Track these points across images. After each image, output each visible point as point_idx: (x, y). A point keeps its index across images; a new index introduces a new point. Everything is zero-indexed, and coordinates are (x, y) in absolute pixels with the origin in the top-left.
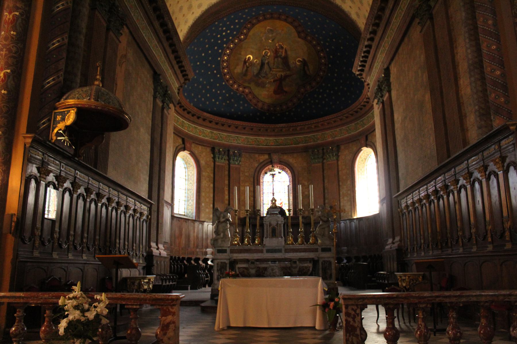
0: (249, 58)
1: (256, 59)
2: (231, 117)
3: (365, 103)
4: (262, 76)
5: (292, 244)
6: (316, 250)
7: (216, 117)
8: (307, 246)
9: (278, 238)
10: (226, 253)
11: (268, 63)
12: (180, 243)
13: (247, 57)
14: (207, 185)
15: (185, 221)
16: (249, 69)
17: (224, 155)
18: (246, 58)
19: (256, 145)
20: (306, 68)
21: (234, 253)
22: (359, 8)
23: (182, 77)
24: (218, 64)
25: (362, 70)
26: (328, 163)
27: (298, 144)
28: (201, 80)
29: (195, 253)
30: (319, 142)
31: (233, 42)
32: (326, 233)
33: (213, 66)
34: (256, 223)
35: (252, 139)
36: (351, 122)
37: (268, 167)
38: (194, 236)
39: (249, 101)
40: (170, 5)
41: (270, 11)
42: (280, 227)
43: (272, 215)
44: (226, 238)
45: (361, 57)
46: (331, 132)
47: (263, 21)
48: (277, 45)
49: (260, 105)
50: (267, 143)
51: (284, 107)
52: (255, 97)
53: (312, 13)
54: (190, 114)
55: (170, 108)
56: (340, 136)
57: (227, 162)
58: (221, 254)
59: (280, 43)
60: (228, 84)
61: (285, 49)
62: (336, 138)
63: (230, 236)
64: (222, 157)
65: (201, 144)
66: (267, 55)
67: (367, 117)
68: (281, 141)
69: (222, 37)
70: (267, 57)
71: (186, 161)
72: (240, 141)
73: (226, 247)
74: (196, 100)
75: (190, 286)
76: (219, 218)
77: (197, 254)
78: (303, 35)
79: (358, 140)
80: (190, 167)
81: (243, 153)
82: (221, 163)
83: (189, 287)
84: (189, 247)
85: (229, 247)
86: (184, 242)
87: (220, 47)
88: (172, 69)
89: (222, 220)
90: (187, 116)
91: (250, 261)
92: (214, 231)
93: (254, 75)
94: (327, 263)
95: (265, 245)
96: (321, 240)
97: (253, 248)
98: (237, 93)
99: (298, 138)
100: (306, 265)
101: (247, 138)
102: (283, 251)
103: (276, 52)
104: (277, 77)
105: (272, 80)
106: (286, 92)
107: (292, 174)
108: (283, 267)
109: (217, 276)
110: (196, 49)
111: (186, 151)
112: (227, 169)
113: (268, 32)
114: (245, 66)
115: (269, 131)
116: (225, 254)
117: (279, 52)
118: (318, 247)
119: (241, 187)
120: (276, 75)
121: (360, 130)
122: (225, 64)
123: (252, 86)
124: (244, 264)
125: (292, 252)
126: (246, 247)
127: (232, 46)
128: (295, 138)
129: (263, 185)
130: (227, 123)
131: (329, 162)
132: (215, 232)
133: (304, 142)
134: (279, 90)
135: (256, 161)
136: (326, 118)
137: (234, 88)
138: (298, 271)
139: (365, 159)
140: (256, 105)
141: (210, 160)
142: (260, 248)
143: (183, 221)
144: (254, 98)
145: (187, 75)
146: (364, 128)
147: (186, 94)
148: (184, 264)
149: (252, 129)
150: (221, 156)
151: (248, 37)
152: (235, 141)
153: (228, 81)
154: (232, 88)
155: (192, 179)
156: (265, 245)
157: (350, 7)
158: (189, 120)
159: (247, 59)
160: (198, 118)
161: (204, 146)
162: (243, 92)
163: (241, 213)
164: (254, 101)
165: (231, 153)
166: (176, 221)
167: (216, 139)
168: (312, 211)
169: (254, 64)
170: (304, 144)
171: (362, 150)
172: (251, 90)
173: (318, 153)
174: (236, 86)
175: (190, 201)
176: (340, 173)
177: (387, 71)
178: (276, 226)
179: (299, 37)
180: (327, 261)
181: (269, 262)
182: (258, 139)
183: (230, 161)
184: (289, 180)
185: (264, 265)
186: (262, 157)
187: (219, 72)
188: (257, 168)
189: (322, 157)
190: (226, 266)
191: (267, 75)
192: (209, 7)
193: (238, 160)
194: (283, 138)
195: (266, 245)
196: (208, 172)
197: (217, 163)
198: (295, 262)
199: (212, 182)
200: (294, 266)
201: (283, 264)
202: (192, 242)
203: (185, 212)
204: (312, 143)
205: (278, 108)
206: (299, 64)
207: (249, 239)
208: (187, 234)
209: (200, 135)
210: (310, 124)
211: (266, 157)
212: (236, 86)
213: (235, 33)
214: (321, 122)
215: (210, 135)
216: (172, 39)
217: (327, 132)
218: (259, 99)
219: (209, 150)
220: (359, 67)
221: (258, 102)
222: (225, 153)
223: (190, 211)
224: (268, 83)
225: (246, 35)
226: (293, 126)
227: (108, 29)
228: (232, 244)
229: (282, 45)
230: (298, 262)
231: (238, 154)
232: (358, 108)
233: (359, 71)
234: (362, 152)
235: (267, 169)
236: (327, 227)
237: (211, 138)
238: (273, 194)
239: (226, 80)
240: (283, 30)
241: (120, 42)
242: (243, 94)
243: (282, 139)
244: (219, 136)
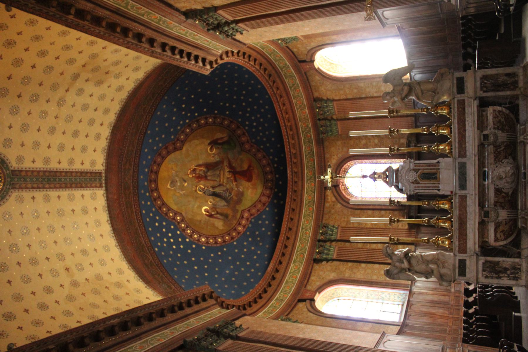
0: (206, 211)
1: (207, 202)
2: (277, 235)
3: (256, 63)
4: (229, 196)
5: (450, 144)
6: (462, 104)
7: (274, 255)
8: (454, 118)
9: (439, 169)
10: (465, 260)
11: (213, 188)
12: (442, 317)
13: (204, 213)
14: (362, 272)
15: (411, 306)
16: (219, 211)
17: (325, 248)
18: (206, 215)
19: (314, 206)
20: (219, 142)
21: (466, 247)
22: (126, 67)
23: (190, 309)
24: (210, 249)
25: (204, 60)
26: (337, 113)
27: (313, 152)
28: (227, 272)
29: (457, 294)
30: (310, 125)
31: (184, 230)
32: (430, 86)
33: (212, 255)
34: (415, 206)
35: (306, 211)
36: (283, 83)
37: (342, 191)
38: (433, 294)
39: (259, 213)
40: (104, 313)
41: (146, 183)
42: (420, 166)
43: (399, 178)
44: (438, 259)
45: (182, 59)
46: (297, 109)
47: (159, 192)
48: (190, 176)
49: (264, 199)
50: (311, 191)
51: (268, 169)
52: (254, 206)
53: (149, 132)
54: (267, 289)
55: (241, 325)
56: (302, 97)
57: (334, 243)
58: (467, 270)
59: (189, 173)
60: (237, 238)
61: (197, 166)
62: (305, 103)
63: (435, 253)
64: (326, 250)
65: (308, 276)
66: (203, 189)
67: (276, 62)
68: (309, 174)
69: (175, 243)
70: (206, 188)
71: (329, 298)
72: (308, 226)
73: (455, 259)
74: (252, 280)
75: (513, 313)
76: (402, 270)
77: (459, 292)
78: (178, 145)
79: (305, 73)
80: (337, 293)
81: (324, 222)
82: (334, 252)
83: (516, 314)
84: (447, 303)
85: (455, 255)
86: (441, 311)
87: (188, 245)
88: (189, 317)
89: (406, 265)
90: (269, 293)
91: (483, 218)
92: (426, 280)
93: (227, 206)
94: (486, 83)
95: (452, 192)
96: (443, 96)
97: (457, 212)
98: (248, 227)
99: (305, 152)
100: (490, 118)
101: (304, 217)
102: (463, 160)
103: (199, 178)
104: (231, 177)
105: (235, 183)
106: (250, 166)
107: (351, 160)
108: (495, 160)
109: (510, 279)
110: (187, 277)
111: (315, 298)
112: (343, 243)
113: (174, 186)
114: (215, 216)
115: (296, 189)
116: (468, 263)
117: (199, 174)
118: (456, 100)
119: (367, 227)
120: (228, 178)
121: (293, 71)
122: (211, 241)
123: (241, 208)
124: (488, 231)
125: (465, 144)
126: (456, 225)
127: (189, 231)
128: (306, 156)
129: (366, 198)
130: (283, 242)
131: (336, 111)
132: (427, 278)
133: (311, 144)
134: (247, 175)
135: (334, 205)
136: (279, 114)
137: (242, 230)
138: (503, 132)
139: (331, 64)
140: (264, 204)
141: (330, 266)
142: (457, 200)
143: (410, 308)
144: (255, 206)
145: (204, 295)
146: (290, 66)
147: (243, 293)
148: (476, 312)
149: (293, 210)
150: (325, 251)
151: (179, 211)
152: (308, 232)
153: (232, 238)
154: (242, 232)
155: (353, 291)
156: (452, 192)
157: (128, 79)
158: (276, 291)
159: (208, 213)
160: (274, 278)
161: (311, 272)
162: (247, 219)
163: (401, 228)
164: (259, 206)
165: (322, 238)
166: (410, 320)
167: (303, 257)
168: (393, 113)
169: (213, 204)
170: (314, 144)
171: (318, 68)
172: (246, 209)
173: (324, 126)
174: (240, 229)
175: (383, 296)
176: (350, 97)
177: (190, 14)
178: (419, 173)
179: (181, 148)
180: (481, 84)
181: (484, 185)
182: (307, 203)
183: (333, 239)
184: (360, 164)
185: (491, 194)
186: (329, 198)
187: (220, 249)
188: (343, 205)
189: (330, 120)
190: (490, 262)
191: (227, 190)
192: (124, 259)
193: (331, 229)
194: (306, 171)
195: (452, 190)
196: (346, 269)
197: (335, 257)
198: (486, 137)
199: (358, 264)
200: (492, 138)
201: (490, 158)
202: (442, 298)
203: (399, 305)
204: (312, 134)
205: (269, 177)
206: (215, 150)
207: (440, 219)
208: (428, 304)
209: (296, 278)
210: (288, 137)
211: (329, 192)
212: (240, 229)
213: (172, 227)
214: (284, 123)
215: (297, 264)
216: (139, 318)
217: (298, 115)
218: (257, 201)
219: (316, 267)
220: (198, 64)
221: (260, 201)
222: (321, 246)
223: (396, 296)
224: (237, 188)
225: (176, 213)
226: (291, 158)
227: (237, 338)
228: (450, 250)
229: (192, 169)
230: (486, 132)
231: (325, 228)
232: (265, 73)
233: (204, 64)
234: (322, 68)
235: (345, 192)
236: (420, 86)
237: (302, 263)
238: (364, 177)
239: (231, 240)
240: (172, 168)
241: (249, 328)
242: (250, 219)
243: (307, 173)
244: (300, 252)
